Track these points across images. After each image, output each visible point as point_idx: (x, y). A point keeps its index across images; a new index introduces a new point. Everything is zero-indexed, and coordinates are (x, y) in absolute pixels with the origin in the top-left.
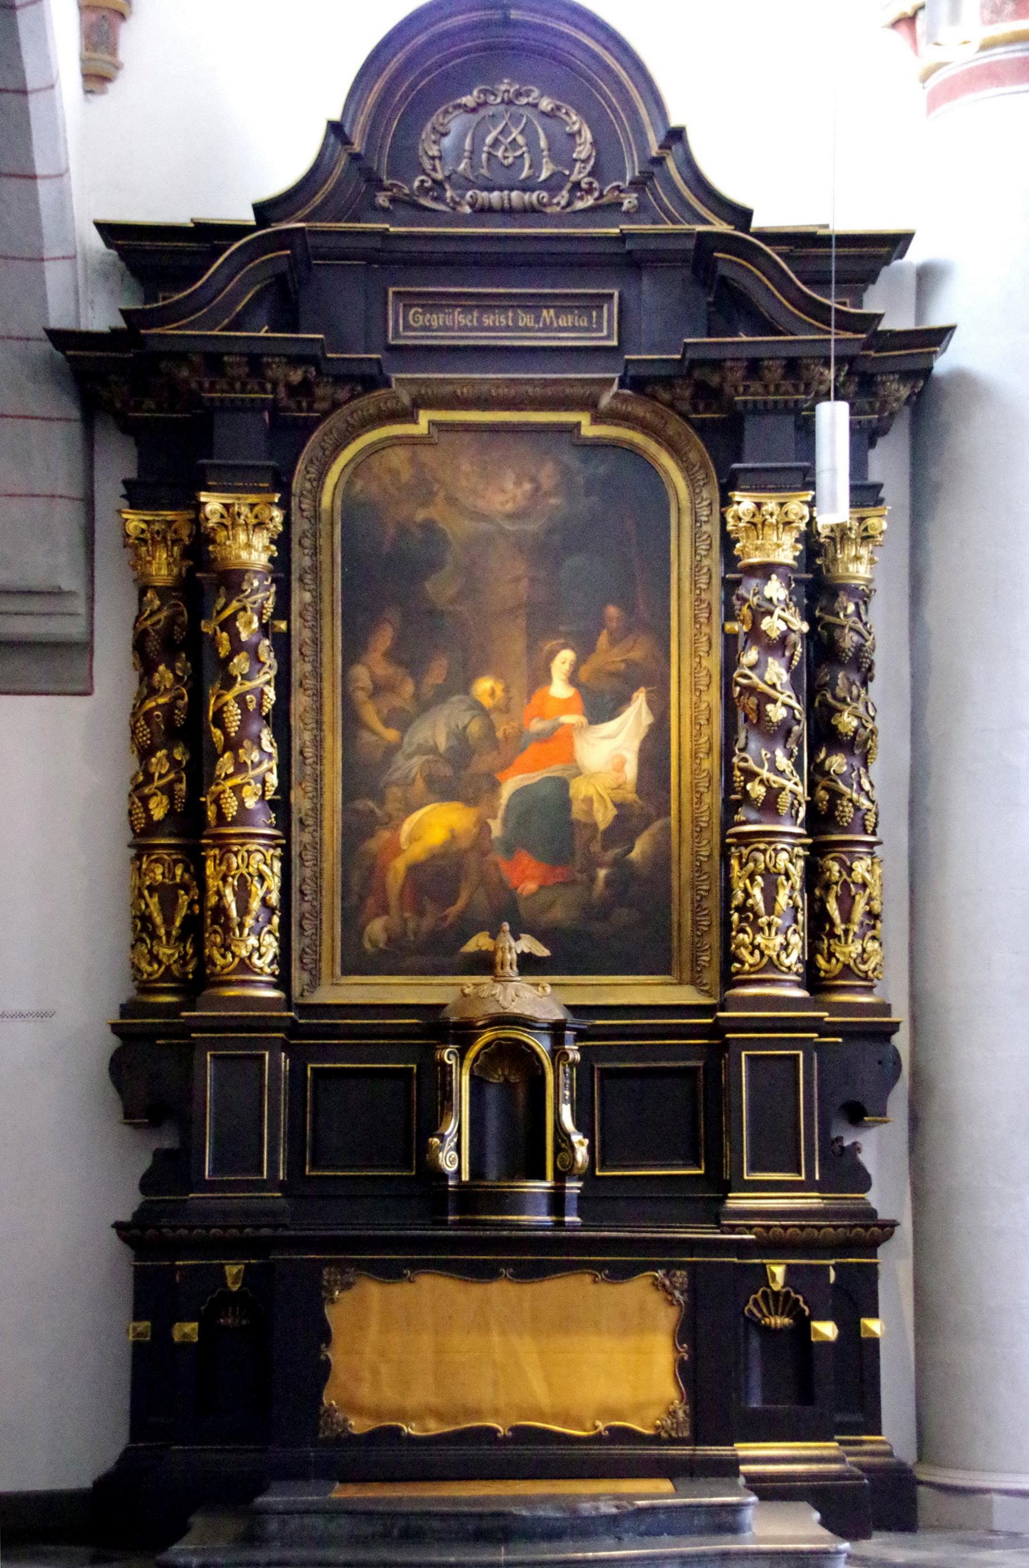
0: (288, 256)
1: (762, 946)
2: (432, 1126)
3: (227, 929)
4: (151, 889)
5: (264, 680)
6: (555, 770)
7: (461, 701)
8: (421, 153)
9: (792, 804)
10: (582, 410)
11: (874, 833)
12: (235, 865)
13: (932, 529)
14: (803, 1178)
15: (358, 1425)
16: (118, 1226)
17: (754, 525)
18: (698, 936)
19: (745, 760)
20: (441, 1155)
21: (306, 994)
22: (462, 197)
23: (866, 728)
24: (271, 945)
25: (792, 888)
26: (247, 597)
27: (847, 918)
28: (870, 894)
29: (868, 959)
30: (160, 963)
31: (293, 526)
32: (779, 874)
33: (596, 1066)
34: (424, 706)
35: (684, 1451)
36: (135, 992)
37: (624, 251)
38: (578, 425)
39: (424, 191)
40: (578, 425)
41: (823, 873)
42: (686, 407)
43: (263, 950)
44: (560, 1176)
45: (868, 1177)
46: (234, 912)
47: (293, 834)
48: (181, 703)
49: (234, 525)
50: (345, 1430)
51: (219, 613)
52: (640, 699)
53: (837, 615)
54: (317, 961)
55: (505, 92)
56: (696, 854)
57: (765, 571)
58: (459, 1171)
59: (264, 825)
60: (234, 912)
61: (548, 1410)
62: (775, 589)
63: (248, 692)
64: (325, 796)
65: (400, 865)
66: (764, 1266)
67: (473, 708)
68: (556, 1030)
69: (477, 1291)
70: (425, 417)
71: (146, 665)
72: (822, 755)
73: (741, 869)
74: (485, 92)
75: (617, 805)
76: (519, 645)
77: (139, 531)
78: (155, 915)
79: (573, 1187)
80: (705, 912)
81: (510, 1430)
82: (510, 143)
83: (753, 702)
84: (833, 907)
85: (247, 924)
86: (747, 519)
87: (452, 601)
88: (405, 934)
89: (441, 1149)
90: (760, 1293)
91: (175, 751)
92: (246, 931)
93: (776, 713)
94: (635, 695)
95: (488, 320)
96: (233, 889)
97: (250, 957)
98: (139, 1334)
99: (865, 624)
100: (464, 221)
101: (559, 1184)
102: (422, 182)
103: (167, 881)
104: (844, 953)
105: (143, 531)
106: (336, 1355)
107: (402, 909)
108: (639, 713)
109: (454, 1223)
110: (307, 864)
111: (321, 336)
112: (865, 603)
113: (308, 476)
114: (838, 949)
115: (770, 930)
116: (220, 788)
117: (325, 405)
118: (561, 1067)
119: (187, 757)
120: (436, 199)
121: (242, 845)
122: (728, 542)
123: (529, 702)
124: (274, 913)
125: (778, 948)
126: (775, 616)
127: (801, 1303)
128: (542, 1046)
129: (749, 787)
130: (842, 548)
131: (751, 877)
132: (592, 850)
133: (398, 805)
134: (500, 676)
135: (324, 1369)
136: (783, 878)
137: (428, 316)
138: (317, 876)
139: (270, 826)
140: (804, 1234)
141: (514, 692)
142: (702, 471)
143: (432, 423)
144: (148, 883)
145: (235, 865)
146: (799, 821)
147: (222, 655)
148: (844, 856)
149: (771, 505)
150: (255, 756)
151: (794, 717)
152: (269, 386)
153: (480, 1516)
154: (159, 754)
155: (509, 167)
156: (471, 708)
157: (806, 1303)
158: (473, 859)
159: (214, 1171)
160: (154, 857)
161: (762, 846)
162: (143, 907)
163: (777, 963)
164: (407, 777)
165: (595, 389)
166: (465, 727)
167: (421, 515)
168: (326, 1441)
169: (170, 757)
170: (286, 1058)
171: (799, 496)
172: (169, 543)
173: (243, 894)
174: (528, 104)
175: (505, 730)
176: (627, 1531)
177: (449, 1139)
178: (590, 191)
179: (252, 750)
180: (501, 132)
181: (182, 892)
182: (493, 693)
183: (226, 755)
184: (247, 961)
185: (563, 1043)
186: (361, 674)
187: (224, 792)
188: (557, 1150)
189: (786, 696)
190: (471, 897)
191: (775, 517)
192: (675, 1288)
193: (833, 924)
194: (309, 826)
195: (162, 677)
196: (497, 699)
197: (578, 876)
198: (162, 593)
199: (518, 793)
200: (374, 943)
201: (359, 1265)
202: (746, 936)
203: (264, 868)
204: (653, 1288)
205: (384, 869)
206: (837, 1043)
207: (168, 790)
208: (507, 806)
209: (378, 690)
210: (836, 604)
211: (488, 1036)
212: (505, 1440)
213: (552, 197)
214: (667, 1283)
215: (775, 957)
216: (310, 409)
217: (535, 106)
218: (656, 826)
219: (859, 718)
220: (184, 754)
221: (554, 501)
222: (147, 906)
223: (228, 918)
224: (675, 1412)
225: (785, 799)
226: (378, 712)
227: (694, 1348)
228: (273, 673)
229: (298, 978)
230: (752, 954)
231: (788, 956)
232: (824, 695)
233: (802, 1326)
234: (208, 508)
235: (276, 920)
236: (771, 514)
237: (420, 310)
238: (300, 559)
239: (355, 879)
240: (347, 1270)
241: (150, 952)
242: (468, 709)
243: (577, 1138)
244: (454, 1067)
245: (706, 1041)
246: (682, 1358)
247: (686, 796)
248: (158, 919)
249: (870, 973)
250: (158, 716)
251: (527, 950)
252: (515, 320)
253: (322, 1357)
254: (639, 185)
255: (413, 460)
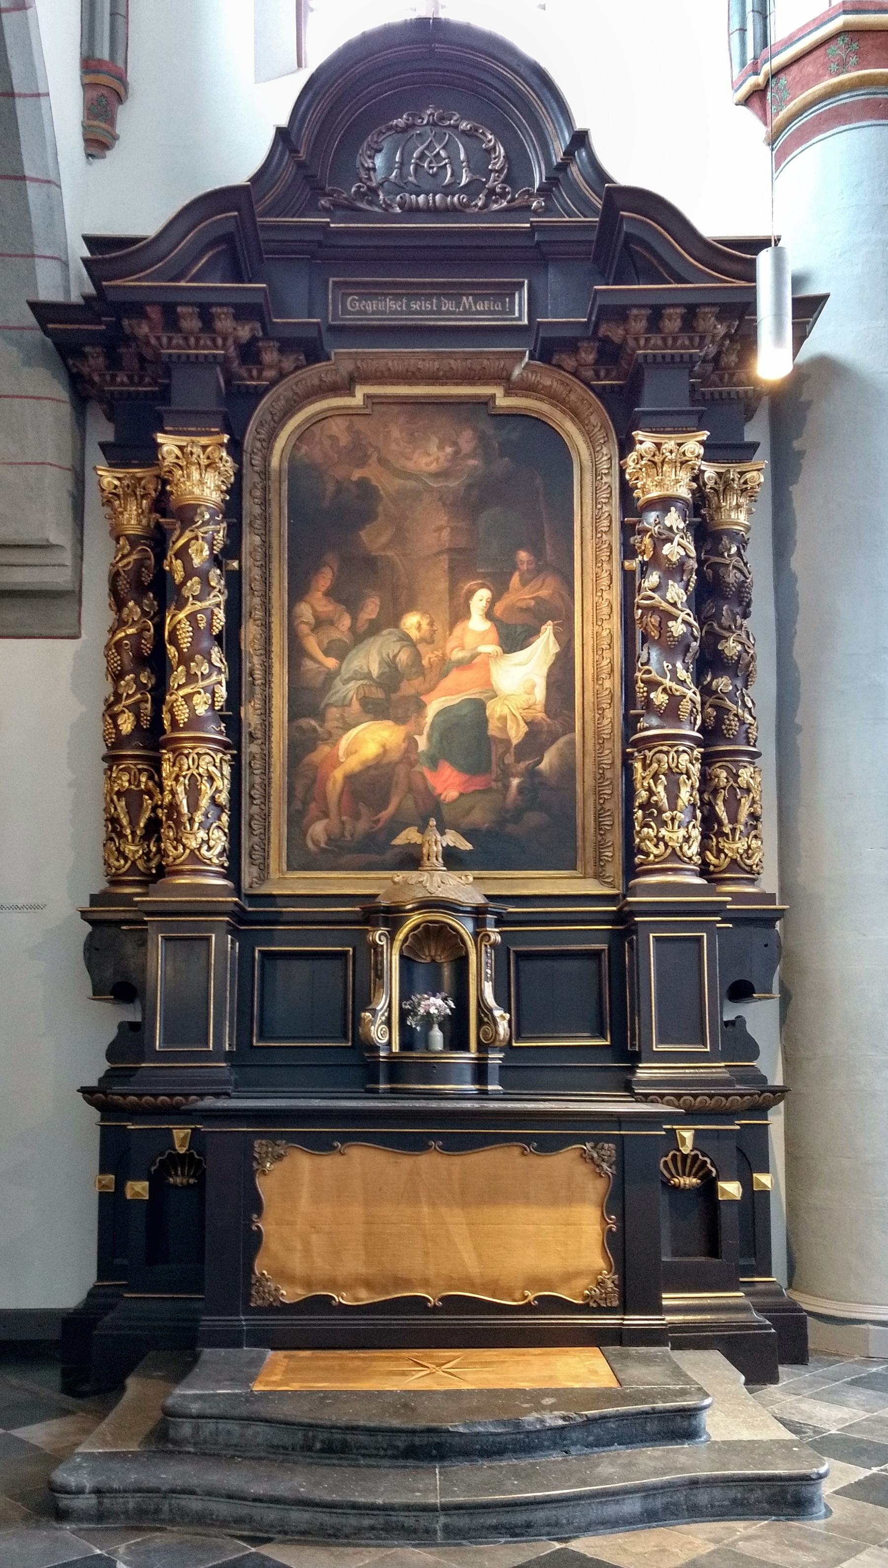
0: (235, 217)
1: (667, 838)
2: (365, 1001)
3: (178, 824)
4: (119, 794)
5: (217, 599)
6: (473, 693)
7: (390, 633)
8: (358, 165)
9: (692, 711)
10: (497, 384)
11: (754, 746)
12: (186, 767)
13: (796, 492)
14: (708, 1050)
15: (289, 1294)
16: (87, 1092)
17: (655, 463)
18: (601, 835)
19: (649, 672)
20: (372, 1028)
21: (255, 885)
22: (393, 200)
23: (748, 653)
24: (219, 840)
25: (692, 787)
26: (198, 528)
27: (734, 819)
28: (753, 798)
29: (753, 854)
30: (126, 859)
31: (244, 479)
32: (682, 774)
33: (512, 949)
34: (359, 637)
35: (611, 1320)
36: (107, 885)
37: (533, 244)
38: (493, 397)
39: (359, 194)
40: (493, 397)
41: (711, 779)
42: (589, 373)
43: (212, 843)
44: (482, 1047)
45: (756, 1045)
46: (185, 810)
47: (243, 744)
48: (147, 634)
49: (190, 463)
50: (276, 1299)
51: (174, 543)
52: (548, 630)
53: (722, 555)
54: (266, 858)
55: (429, 115)
56: (598, 764)
57: (664, 504)
58: (389, 1043)
59: (215, 731)
60: (185, 810)
61: (478, 1281)
62: (674, 519)
63: (198, 612)
64: (273, 715)
65: (338, 775)
66: (675, 1130)
67: (403, 640)
68: (478, 914)
69: (407, 1162)
70: (361, 391)
71: (119, 603)
72: (709, 679)
73: (644, 770)
74: (413, 116)
75: (527, 723)
76: (443, 585)
77: (112, 487)
78: (122, 816)
79: (495, 1058)
80: (608, 813)
81: (440, 1300)
82: (435, 156)
83: (655, 620)
84: (721, 810)
85: (197, 819)
86: (649, 457)
87: (385, 547)
88: (343, 835)
89: (373, 1023)
90: (670, 1155)
91: (142, 675)
92: (196, 825)
93: (677, 628)
94: (543, 627)
95: (415, 306)
96: (185, 788)
97: (199, 849)
98: (104, 1186)
99: (746, 564)
100: (395, 218)
101: (481, 1056)
102: (359, 187)
103: (133, 787)
104: (729, 849)
105: (116, 487)
106: (266, 1225)
107: (340, 815)
108: (547, 643)
109: (386, 1091)
110: (255, 772)
111: (264, 285)
112: (744, 547)
113: (259, 436)
114: (726, 845)
115: (673, 824)
116: (174, 697)
117: (270, 374)
118: (483, 948)
119: (153, 681)
120: (370, 203)
121: (193, 748)
122: (626, 490)
123: (451, 634)
124: (223, 811)
125: (681, 840)
126: (675, 543)
127: (709, 1166)
128: (466, 928)
129: (652, 695)
130: (725, 499)
131: (655, 777)
132: (506, 762)
133: (336, 724)
134: (424, 613)
135: (254, 1241)
136: (685, 776)
137: (364, 302)
138: (266, 785)
139: (220, 733)
140: (713, 1101)
141: (437, 626)
142: (603, 431)
143: (367, 397)
144: (116, 789)
145: (186, 767)
146: (696, 728)
147: (177, 582)
148: (730, 765)
149: (669, 444)
150: (205, 669)
151: (692, 634)
152: (220, 341)
153: (413, 1432)
154: (127, 678)
155: (434, 175)
156: (401, 639)
157: (713, 1165)
158: (401, 770)
159: (166, 1040)
160: (121, 767)
161: (665, 748)
162: (113, 810)
163: (680, 854)
164: (345, 697)
165: (509, 362)
166: (395, 656)
167: (356, 475)
168: (259, 1310)
169: (136, 680)
170: (233, 942)
171: (696, 436)
172: (139, 497)
173: (193, 793)
174: (450, 126)
175: (430, 658)
176: (574, 1444)
177: (380, 1013)
178: (503, 195)
179: (203, 663)
180: (427, 148)
181: (147, 797)
182: (419, 627)
183: (180, 669)
184: (197, 853)
185: (484, 926)
186: (305, 610)
187: (177, 700)
188: (480, 1023)
189: (685, 614)
190: (400, 803)
191: (674, 454)
192: (603, 1160)
193: (721, 824)
194: (257, 739)
195: (131, 611)
196: (423, 632)
197: (494, 784)
198: (133, 541)
199: (439, 714)
200: (316, 843)
201: (291, 1138)
202: (650, 830)
203: (212, 769)
204: (581, 1160)
205: (325, 779)
206: (729, 928)
207: (135, 709)
208: (432, 724)
209: (320, 623)
210: (720, 546)
211: (415, 919)
212: (435, 1310)
213: (470, 200)
214: (595, 1155)
215: (678, 849)
216: (259, 378)
217: (456, 127)
218: (562, 741)
219: (743, 644)
220: (149, 678)
221: (472, 462)
222: (116, 809)
223: (180, 814)
224: (603, 1282)
225: (686, 706)
226: (319, 644)
227: (622, 1219)
228: (222, 599)
229: (248, 873)
230: (656, 846)
231: (689, 848)
232: (712, 624)
233: (709, 1186)
234: (165, 449)
235: (225, 818)
236: (671, 452)
237: (356, 298)
238: (250, 507)
239: (299, 792)
240: (278, 1142)
241: (118, 849)
242: (398, 641)
243: (498, 1013)
244: (385, 947)
245: (610, 927)
246: (610, 1229)
247: (589, 715)
248: (125, 822)
249: (754, 867)
250: (126, 644)
251: (451, 844)
252: (439, 306)
253: (254, 1228)
254: (545, 191)
255: (349, 429)
